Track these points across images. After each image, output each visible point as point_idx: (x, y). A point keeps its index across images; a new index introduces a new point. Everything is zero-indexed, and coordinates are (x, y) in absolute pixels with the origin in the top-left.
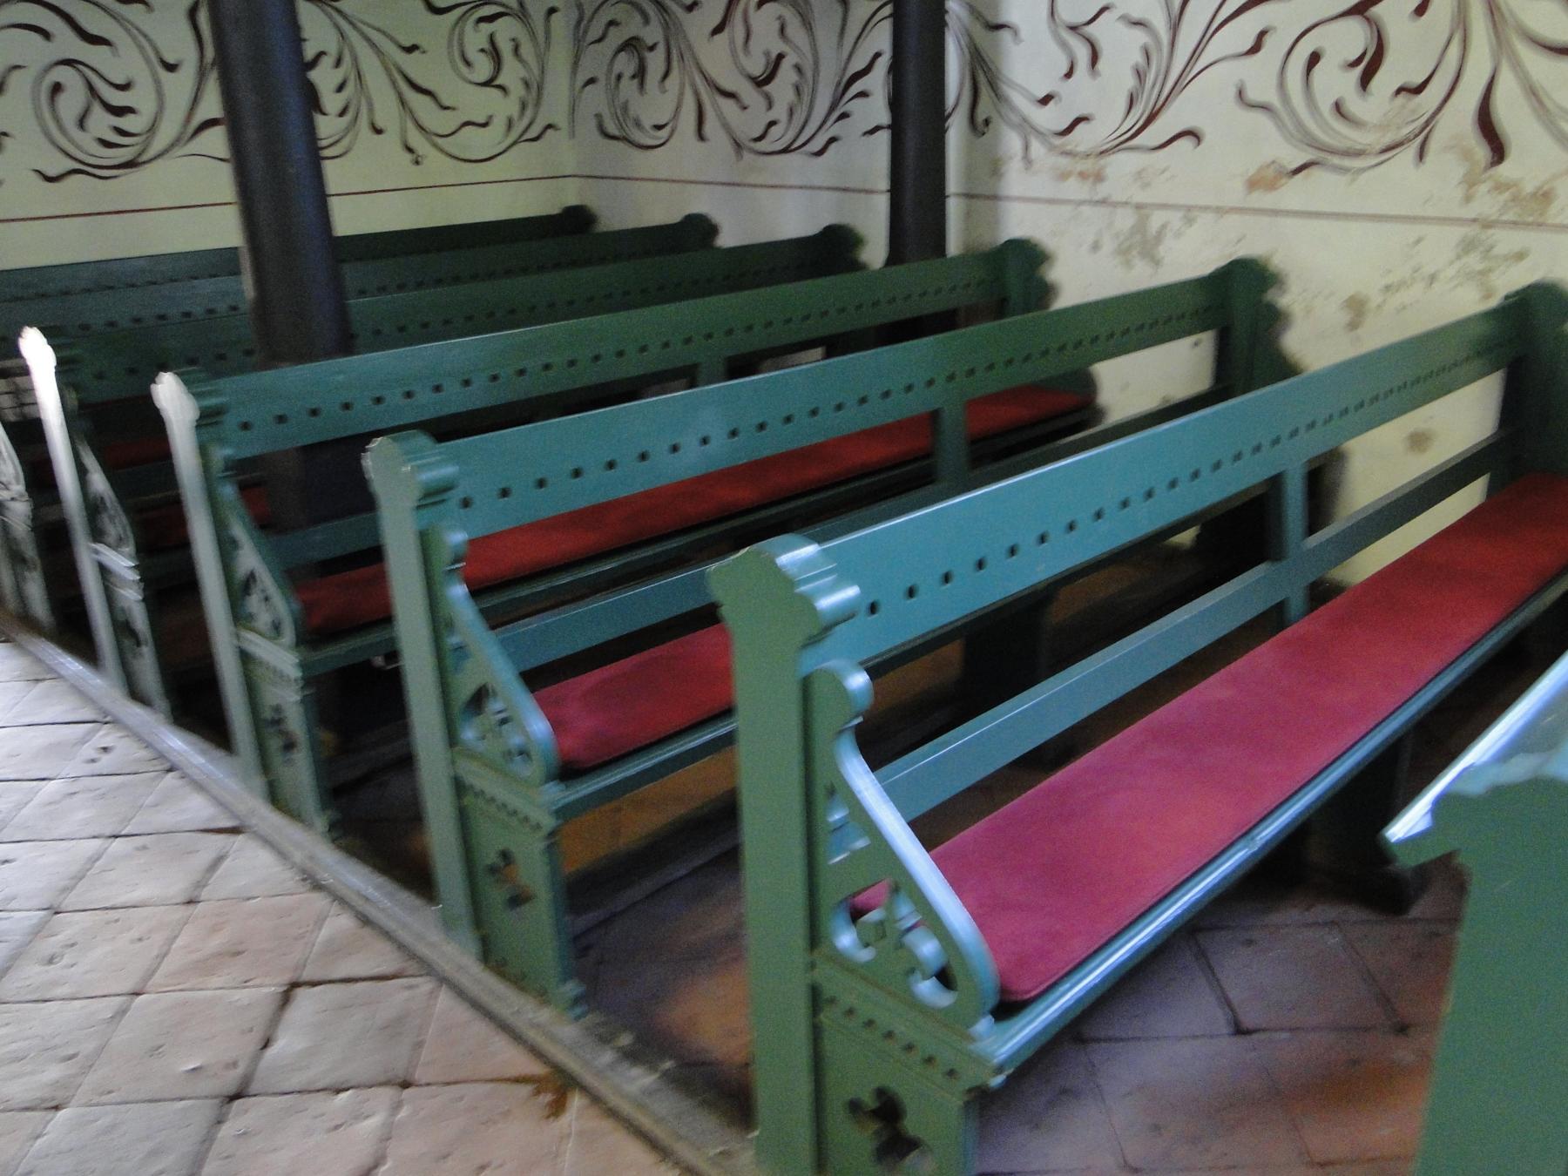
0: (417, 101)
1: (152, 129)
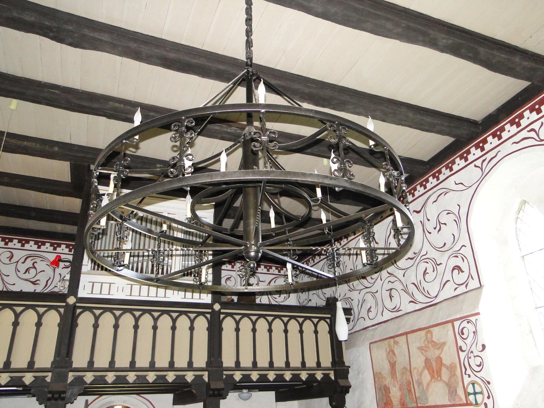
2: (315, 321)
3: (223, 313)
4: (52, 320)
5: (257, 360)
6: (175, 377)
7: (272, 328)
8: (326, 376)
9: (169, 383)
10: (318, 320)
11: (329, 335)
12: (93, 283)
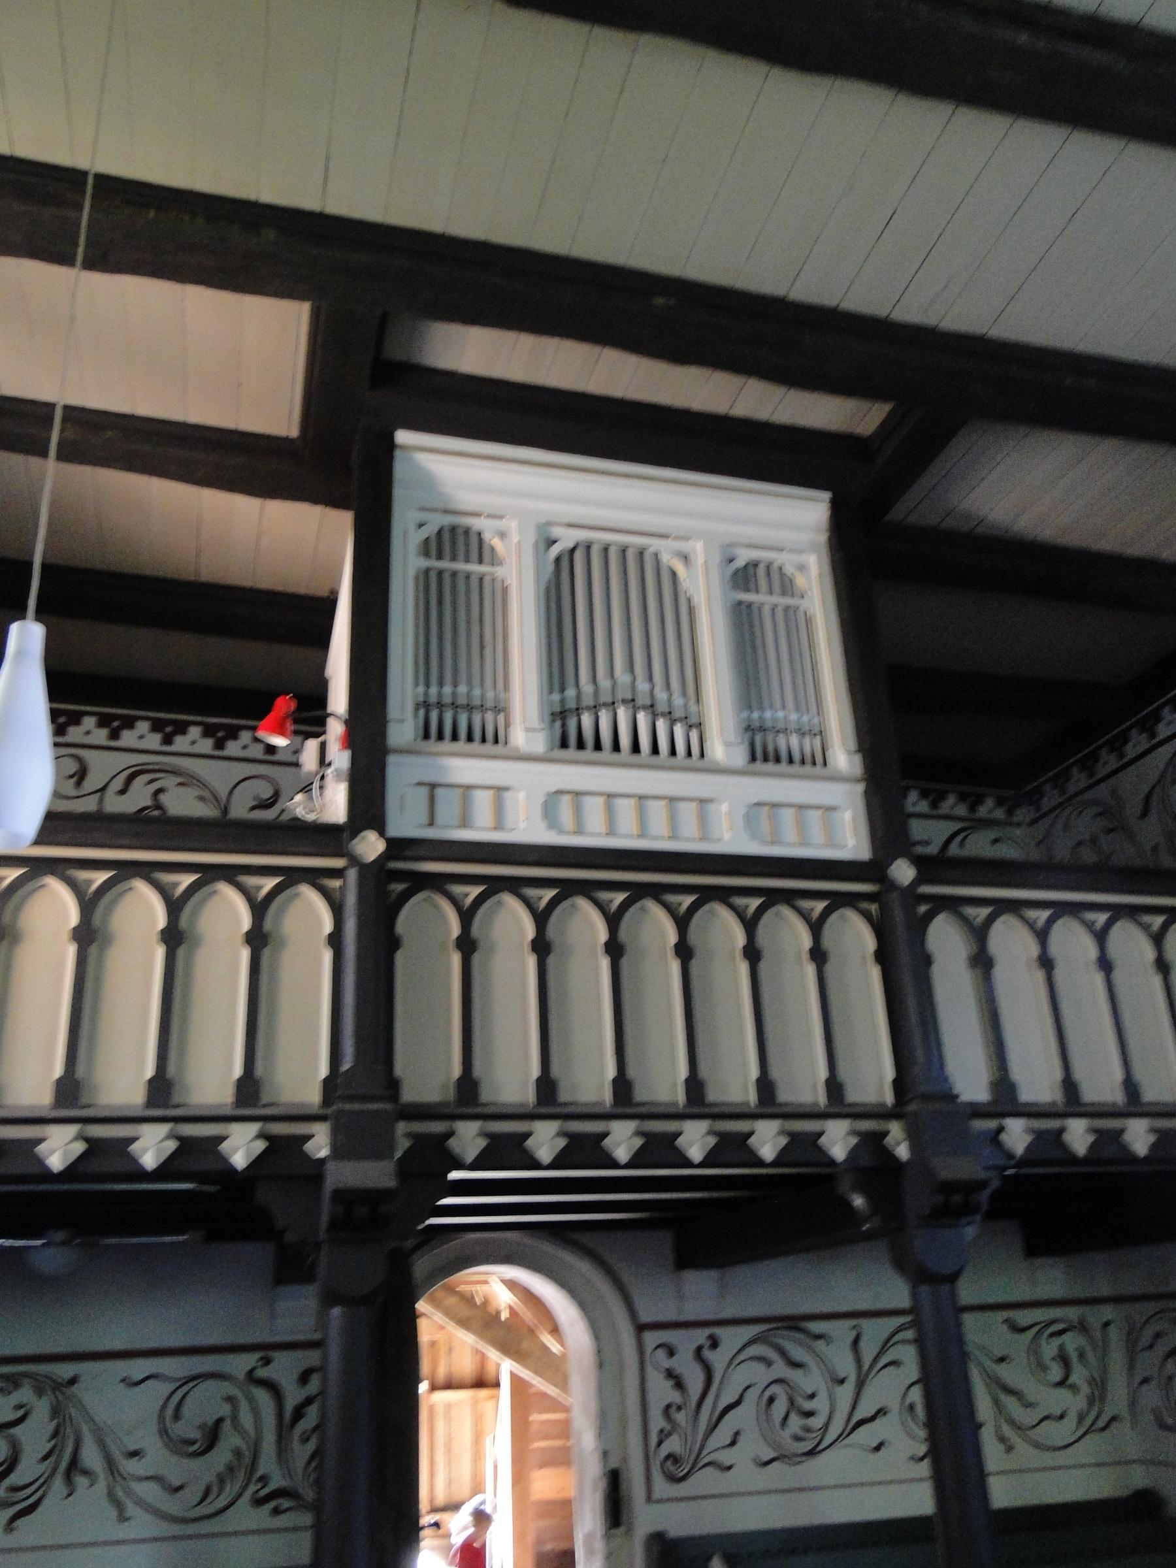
0: (1010, 1403)
1: (826, 1426)
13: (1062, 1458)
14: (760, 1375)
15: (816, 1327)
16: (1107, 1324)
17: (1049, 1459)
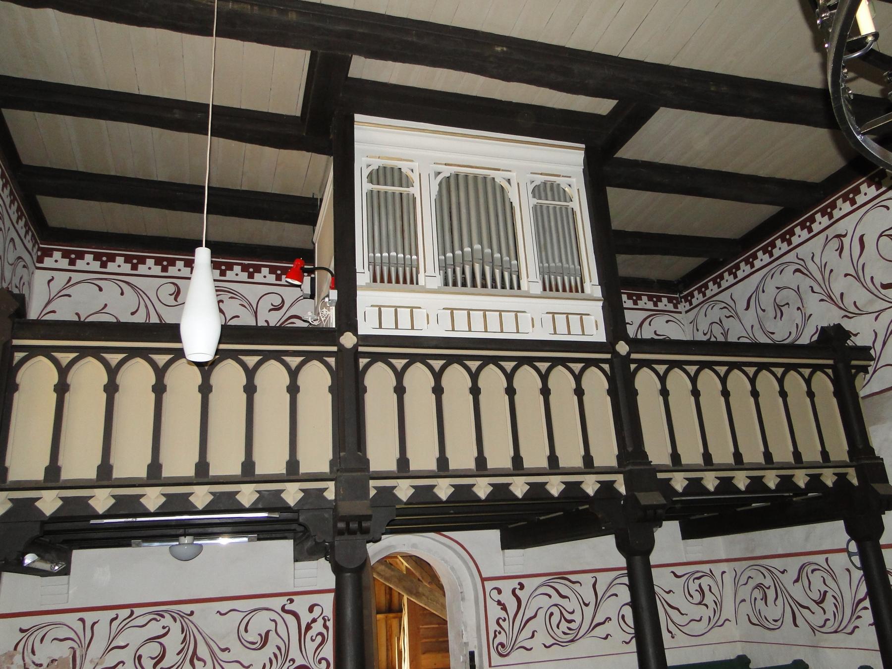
0: (673, 613)
2: (661, 369)
3: (365, 355)
4: (317, 379)
5: (449, 454)
6: (163, 500)
7: (550, 386)
8: (842, 479)
9: (441, 502)
10: (666, 367)
11: (609, 398)
12: (380, 310)
13: (699, 640)
14: (545, 602)
15: (572, 577)
16: (724, 572)
17: (695, 641)
